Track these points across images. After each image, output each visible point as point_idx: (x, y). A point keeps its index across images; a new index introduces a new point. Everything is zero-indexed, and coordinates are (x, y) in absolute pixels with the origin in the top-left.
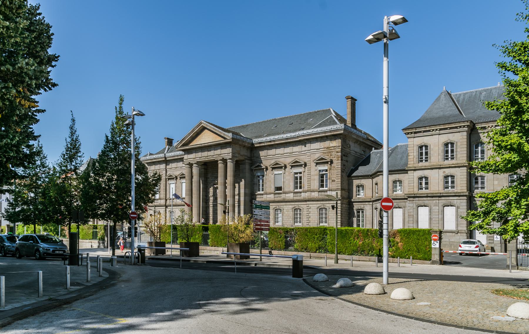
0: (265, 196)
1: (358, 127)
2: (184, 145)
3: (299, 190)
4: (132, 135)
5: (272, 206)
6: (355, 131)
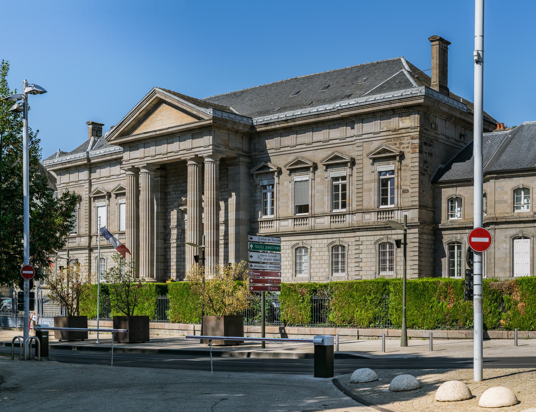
0: (275, 224)
1: (453, 89)
2: (122, 135)
3: (340, 210)
4: (24, 129)
5: (286, 244)
6: (446, 99)
